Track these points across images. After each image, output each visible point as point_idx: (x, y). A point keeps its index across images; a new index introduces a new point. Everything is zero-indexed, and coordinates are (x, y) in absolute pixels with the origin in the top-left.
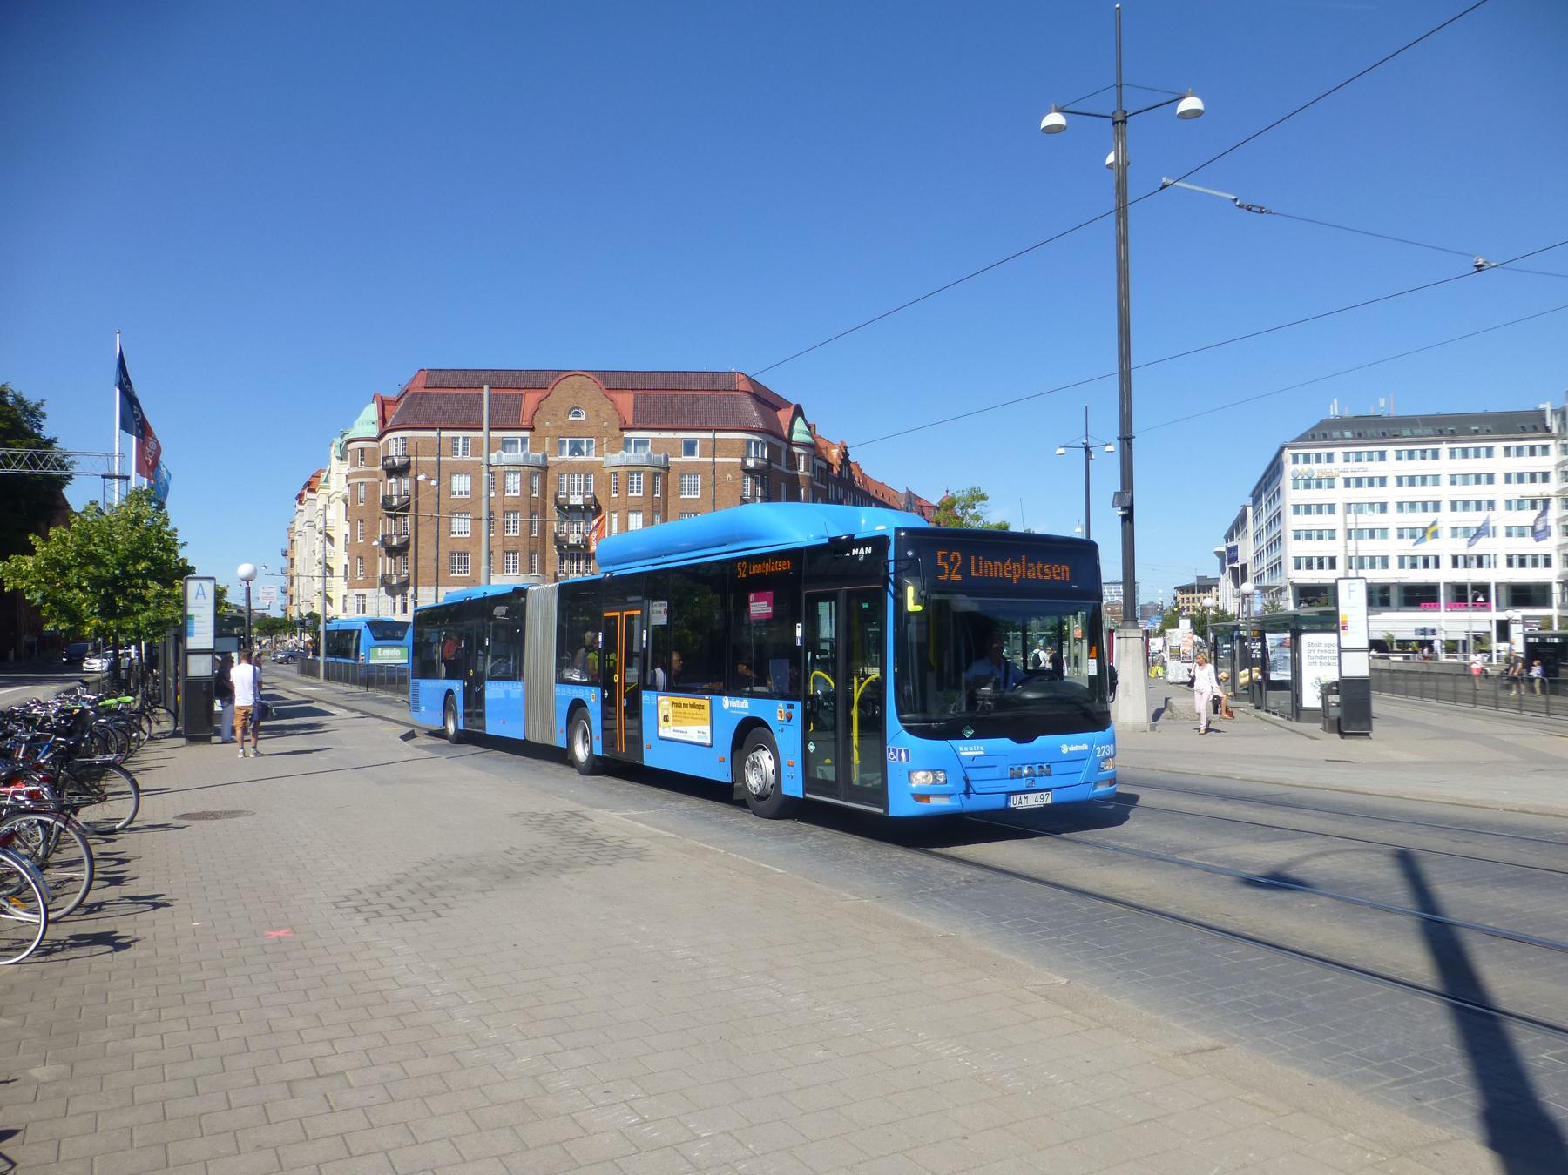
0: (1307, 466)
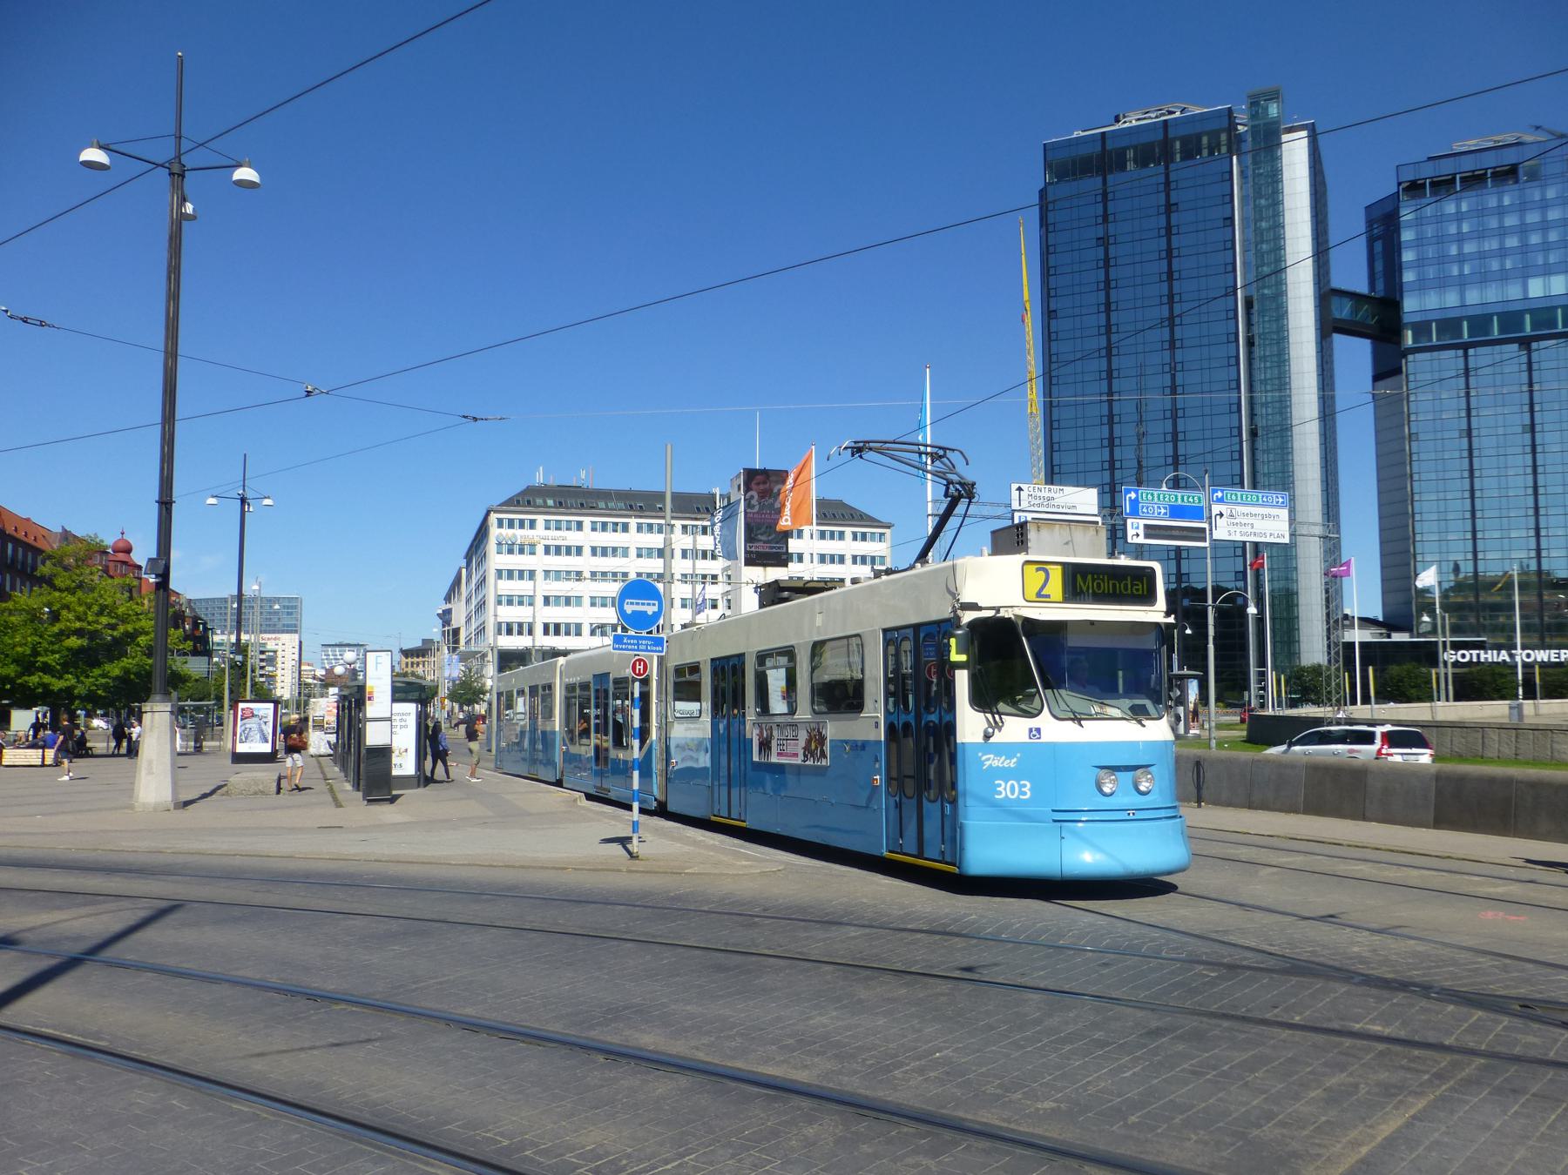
0: (511, 532)
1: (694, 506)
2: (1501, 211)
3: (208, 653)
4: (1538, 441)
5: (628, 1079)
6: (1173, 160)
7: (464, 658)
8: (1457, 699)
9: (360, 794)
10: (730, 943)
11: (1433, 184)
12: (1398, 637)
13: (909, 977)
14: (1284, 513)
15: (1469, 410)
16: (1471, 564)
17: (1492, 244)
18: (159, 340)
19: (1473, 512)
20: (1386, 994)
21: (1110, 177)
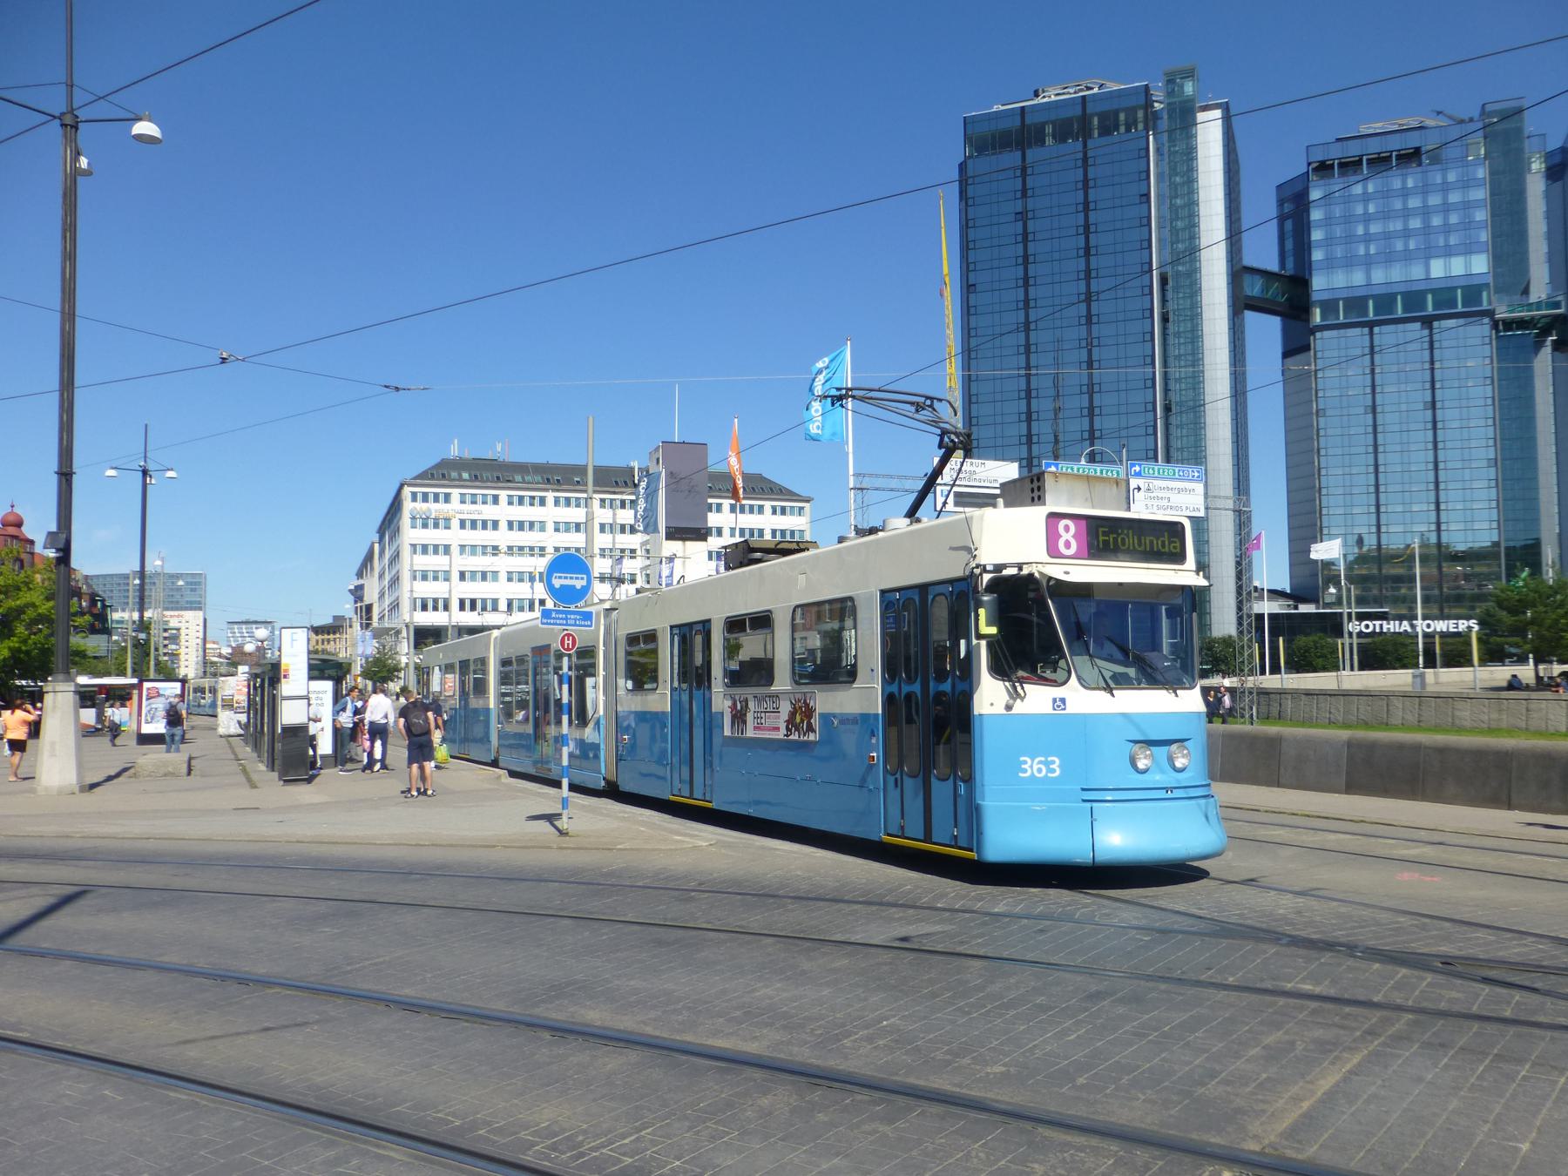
0: (425, 506)
1: (614, 480)
2: (1405, 193)
3: (107, 631)
4: (1439, 418)
5: (577, 1055)
6: (1091, 136)
7: (378, 634)
8: (1361, 668)
9: (276, 774)
10: (668, 917)
11: (1341, 165)
12: (1304, 608)
13: (850, 948)
14: (1200, 487)
15: (1373, 387)
16: (1374, 537)
17: (1397, 225)
18: (55, 299)
19: (1377, 486)
20: (1313, 954)
21: (1029, 153)
